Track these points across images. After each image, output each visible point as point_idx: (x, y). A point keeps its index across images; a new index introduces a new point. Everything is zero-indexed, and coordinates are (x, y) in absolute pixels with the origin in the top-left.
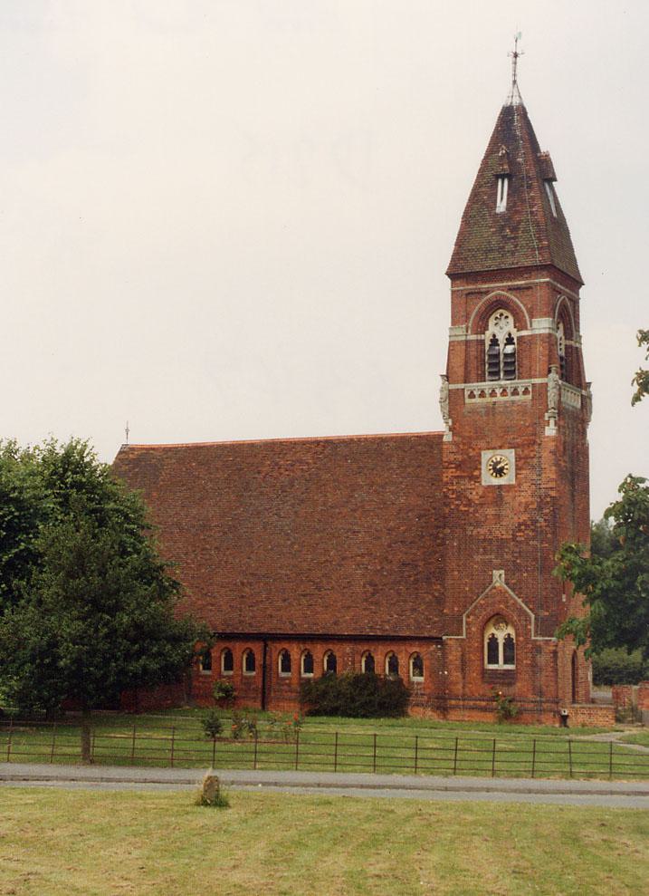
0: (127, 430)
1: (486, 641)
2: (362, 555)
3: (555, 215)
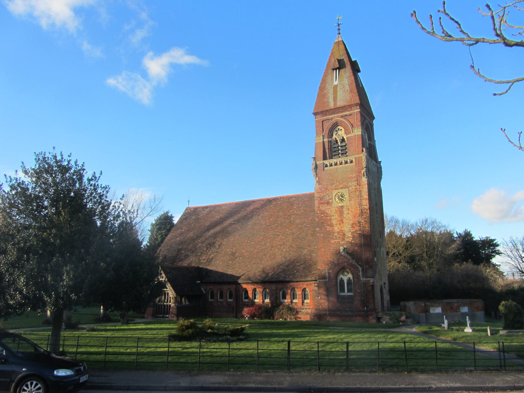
0: (189, 201)
1: (339, 281)
2: (281, 245)
3: (361, 86)
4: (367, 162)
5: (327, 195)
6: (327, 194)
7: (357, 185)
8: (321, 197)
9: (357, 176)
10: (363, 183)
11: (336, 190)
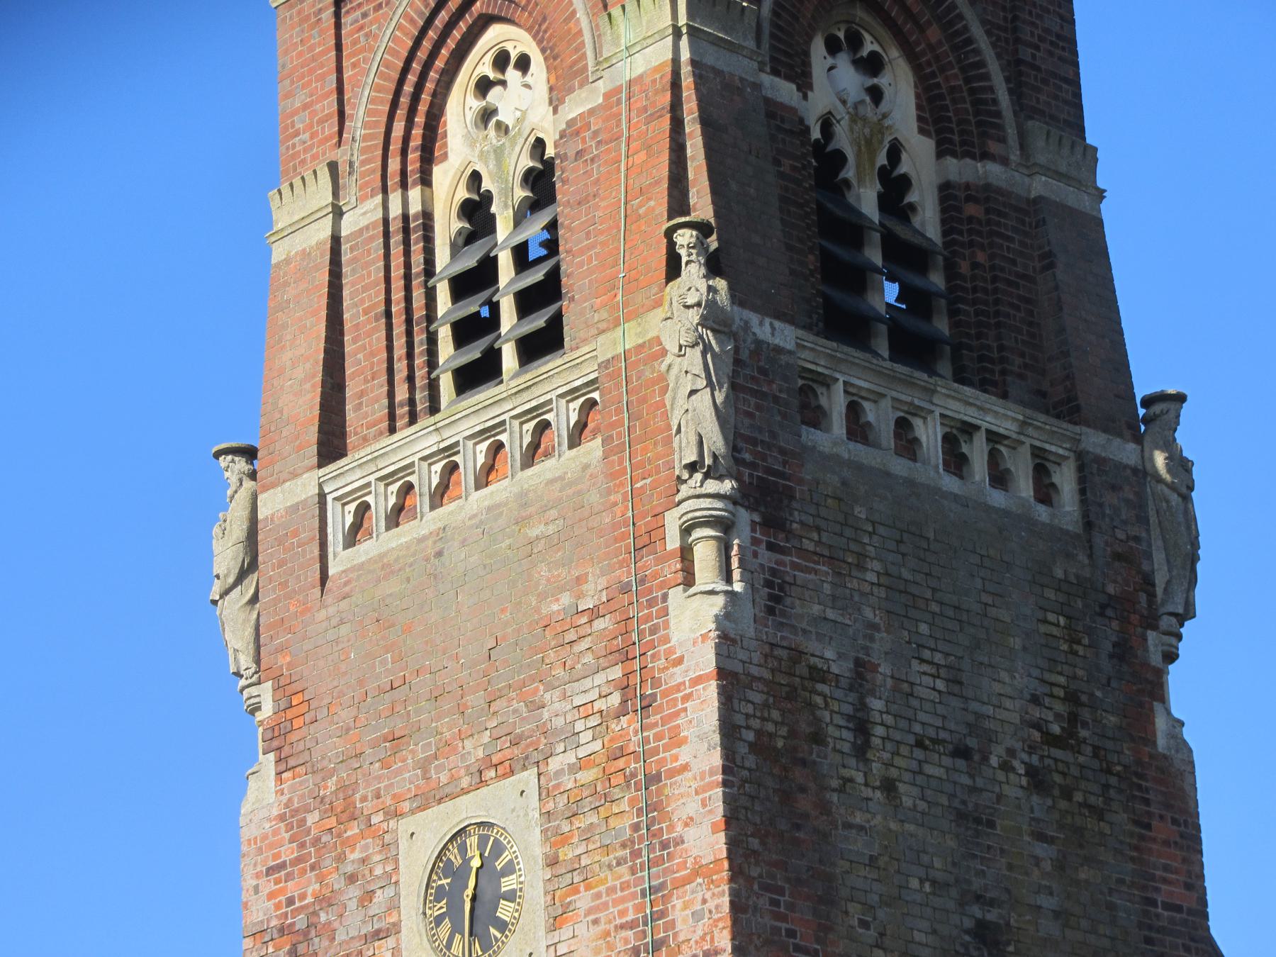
4: (895, 443)
5: (354, 892)
6: (352, 879)
7: (622, 712)
8: (300, 922)
9: (625, 589)
10: (678, 675)
11: (435, 810)
